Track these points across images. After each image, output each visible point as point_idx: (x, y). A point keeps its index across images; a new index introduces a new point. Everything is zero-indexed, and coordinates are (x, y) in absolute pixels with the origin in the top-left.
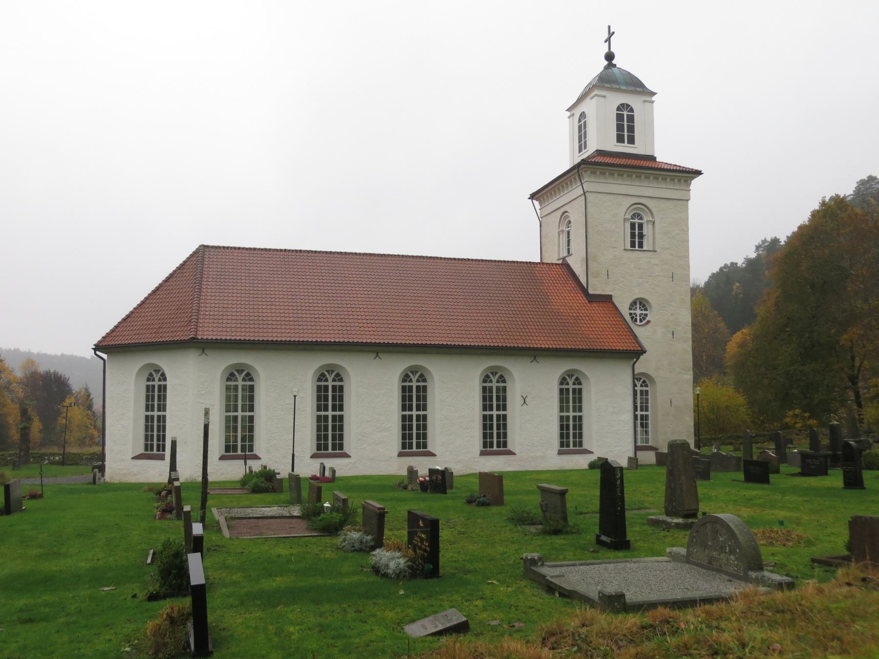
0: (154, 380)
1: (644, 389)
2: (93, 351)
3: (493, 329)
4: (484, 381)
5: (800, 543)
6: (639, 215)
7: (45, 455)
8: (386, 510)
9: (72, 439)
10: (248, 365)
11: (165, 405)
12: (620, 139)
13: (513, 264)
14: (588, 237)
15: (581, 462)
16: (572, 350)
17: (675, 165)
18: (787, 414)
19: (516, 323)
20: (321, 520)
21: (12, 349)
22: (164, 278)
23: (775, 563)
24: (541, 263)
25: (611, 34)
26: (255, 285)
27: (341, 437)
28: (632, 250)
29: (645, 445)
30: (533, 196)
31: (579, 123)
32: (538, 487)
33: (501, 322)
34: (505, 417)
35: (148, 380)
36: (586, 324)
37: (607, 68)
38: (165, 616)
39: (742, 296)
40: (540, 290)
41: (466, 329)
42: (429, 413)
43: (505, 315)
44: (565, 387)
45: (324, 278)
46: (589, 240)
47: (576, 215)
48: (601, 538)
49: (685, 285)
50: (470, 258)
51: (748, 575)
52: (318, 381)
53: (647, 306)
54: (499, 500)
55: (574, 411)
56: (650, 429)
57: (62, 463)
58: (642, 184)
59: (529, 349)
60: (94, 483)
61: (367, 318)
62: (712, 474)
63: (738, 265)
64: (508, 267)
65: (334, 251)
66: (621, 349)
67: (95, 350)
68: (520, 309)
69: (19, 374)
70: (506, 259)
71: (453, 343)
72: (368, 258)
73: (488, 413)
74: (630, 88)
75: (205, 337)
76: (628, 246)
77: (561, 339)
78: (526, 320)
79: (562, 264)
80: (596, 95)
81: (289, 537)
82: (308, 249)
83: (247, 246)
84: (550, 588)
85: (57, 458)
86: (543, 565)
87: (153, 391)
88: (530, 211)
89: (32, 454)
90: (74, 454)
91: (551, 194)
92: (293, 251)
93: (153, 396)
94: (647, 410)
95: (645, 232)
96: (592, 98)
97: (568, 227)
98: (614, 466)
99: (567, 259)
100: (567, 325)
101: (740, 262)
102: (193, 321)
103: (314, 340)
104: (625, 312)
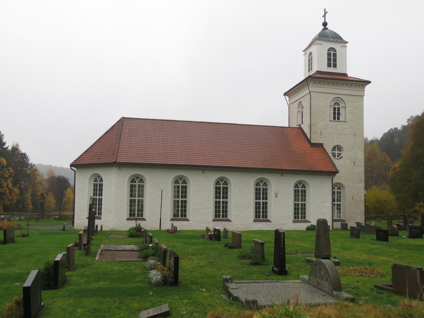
0: (97, 181)
1: (339, 191)
2: (70, 167)
3: (261, 160)
4: (257, 185)
5: (377, 275)
6: (338, 103)
7: (51, 215)
8: (168, 250)
9: (70, 208)
10: (185, 176)
11: (102, 193)
12: (329, 65)
13: (274, 128)
14: (311, 114)
15: (303, 226)
16: (300, 171)
17: (357, 78)
18: (416, 205)
19: (273, 157)
20: (144, 253)
21: (48, 165)
22: (104, 133)
23: (354, 287)
24: (289, 127)
25: (326, 13)
26: (146, 137)
27: (185, 211)
28: (338, 121)
29: (339, 219)
30: (285, 94)
31: (309, 57)
32: (253, 240)
33: (266, 156)
34: (266, 203)
35: (95, 181)
36: (309, 158)
37: (323, 30)
38: (14, 301)
39: (399, 144)
40: (286, 141)
41: (248, 159)
42: (228, 200)
43: (268, 153)
44: (297, 189)
45: (198, 134)
46: (312, 116)
47: (306, 103)
48: (274, 269)
49: (361, 139)
50: (253, 124)
51: (333, 293)
52: (295, 188)
53: (341, 149)
54: (239, 246)
55: (302, 201)
56: (341, 211)
57: (59, 219)
58: (335, 88)
59: (279, 170)
60: (64, 229)
61: (200, 153)
62: (361, 235)
63: (398, 129)
64: (271, 129)
65: (186, 120)
66: (326, 170)
67: (71, 166)
68: (276, 150)
69: (46, 177)
70: (270, 125)
71: (241, 166)
72: (202, 124)
73: (258, 201)
74: (335, 40)
75: (121, 161)
76: (332, 119)
77: (295, 165)
78: (278, 155)
79: (299, 128)
80: (317, 44)
81: (126, 261)
82: (173, 120)
83: (144, 118)
84: (230, 295)
85: (57, 217)
86: (232, 282)
87: (97, 186)
88: (284, 101)
89: (46, 214)
90: (65, 215)
91: (294, 93)
92: (166, 120)
93: (97, 189)
94: (340, 201)
95: (341, 112)
96: (315, 45)
97: (302, 109)
98: (280, 231)
99: (301, 125)
100: (299, 158)
101: (399, 127)
102: (115, 153)
103: (173, 163)
104: (330, 152)
